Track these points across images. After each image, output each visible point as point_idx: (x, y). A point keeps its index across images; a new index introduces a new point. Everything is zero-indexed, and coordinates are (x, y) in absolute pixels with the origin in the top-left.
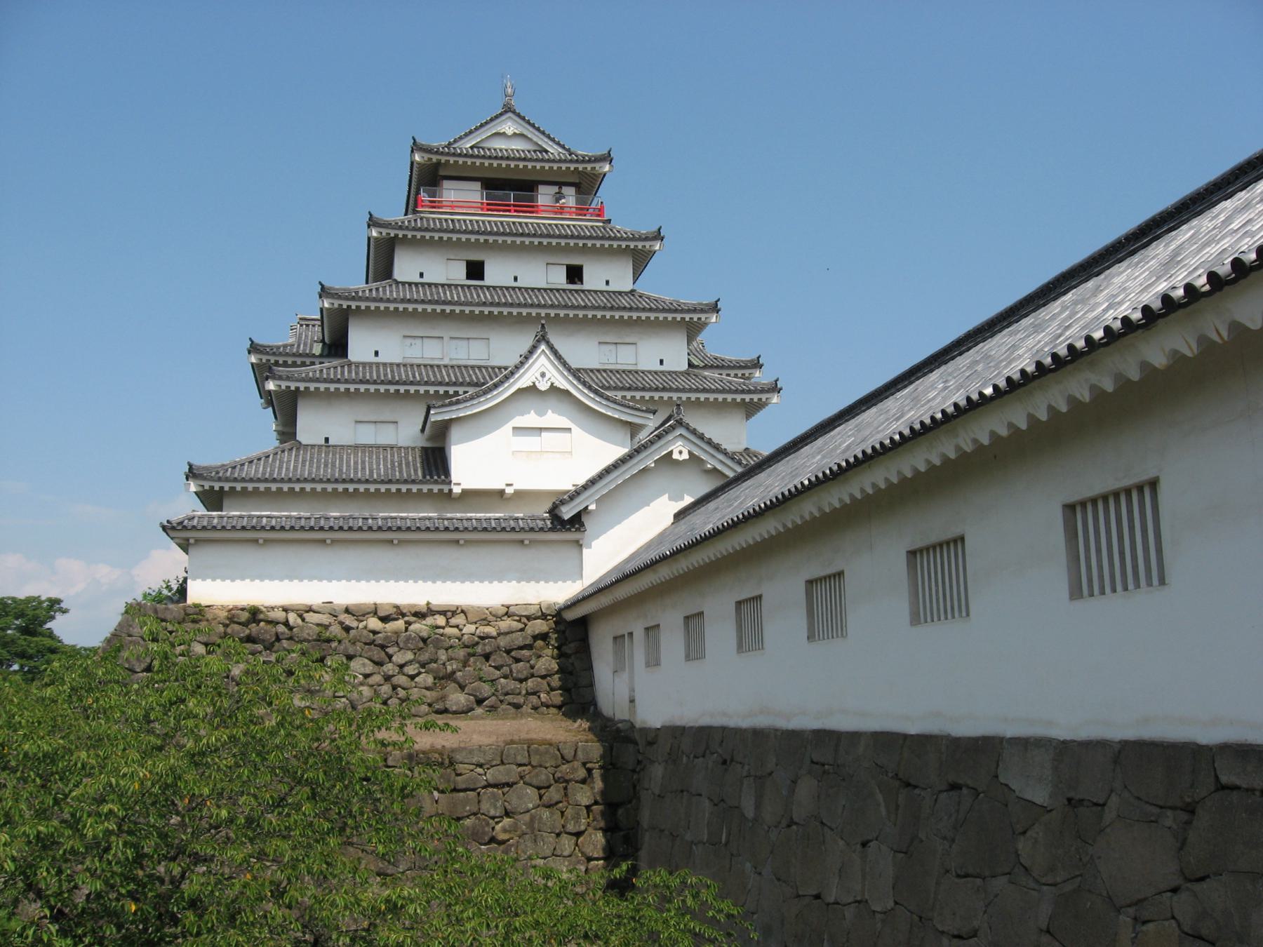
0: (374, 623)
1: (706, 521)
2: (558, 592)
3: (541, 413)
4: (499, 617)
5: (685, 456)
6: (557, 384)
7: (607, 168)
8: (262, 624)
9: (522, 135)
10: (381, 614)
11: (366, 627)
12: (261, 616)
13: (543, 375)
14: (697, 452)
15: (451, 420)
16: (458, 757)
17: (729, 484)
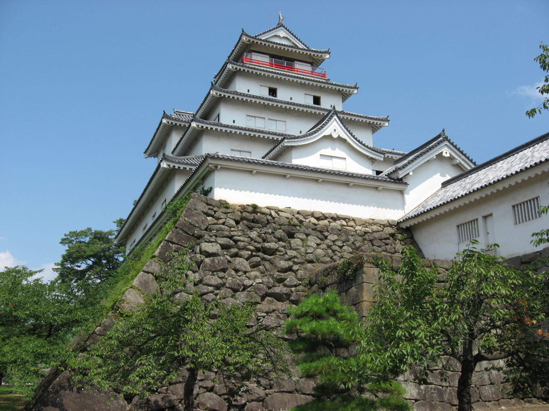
0: (313, 220)
1: (458, 189)
2: (395, 215)
3: (334, 149)
4: (371, 224)
5: (448, 155)
6: (342, 137)
7: (328, 56)
8: (259, 214)
9: (286, 38)
10: (317, 216)
11: (310, 222)
12: (258, 210)
13: (335, 130)
14: (453, 154)
15: (292, 147)
16: (438, 264)
17: (465, 174)
